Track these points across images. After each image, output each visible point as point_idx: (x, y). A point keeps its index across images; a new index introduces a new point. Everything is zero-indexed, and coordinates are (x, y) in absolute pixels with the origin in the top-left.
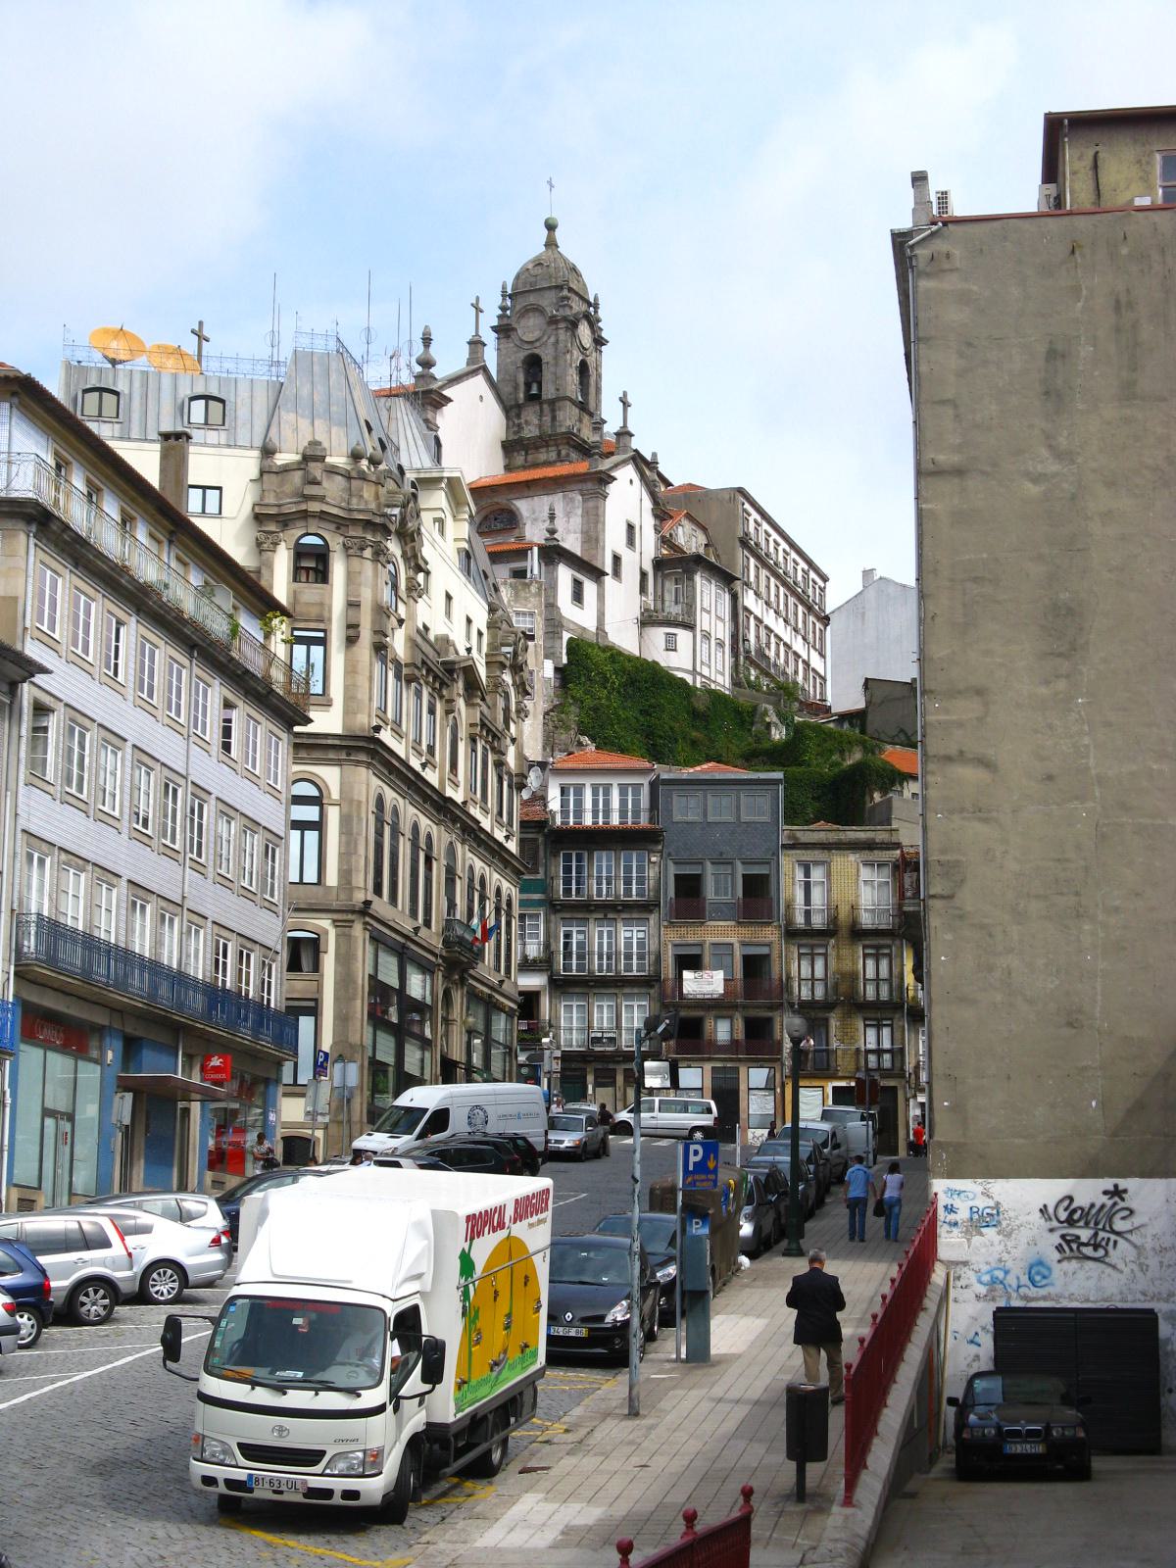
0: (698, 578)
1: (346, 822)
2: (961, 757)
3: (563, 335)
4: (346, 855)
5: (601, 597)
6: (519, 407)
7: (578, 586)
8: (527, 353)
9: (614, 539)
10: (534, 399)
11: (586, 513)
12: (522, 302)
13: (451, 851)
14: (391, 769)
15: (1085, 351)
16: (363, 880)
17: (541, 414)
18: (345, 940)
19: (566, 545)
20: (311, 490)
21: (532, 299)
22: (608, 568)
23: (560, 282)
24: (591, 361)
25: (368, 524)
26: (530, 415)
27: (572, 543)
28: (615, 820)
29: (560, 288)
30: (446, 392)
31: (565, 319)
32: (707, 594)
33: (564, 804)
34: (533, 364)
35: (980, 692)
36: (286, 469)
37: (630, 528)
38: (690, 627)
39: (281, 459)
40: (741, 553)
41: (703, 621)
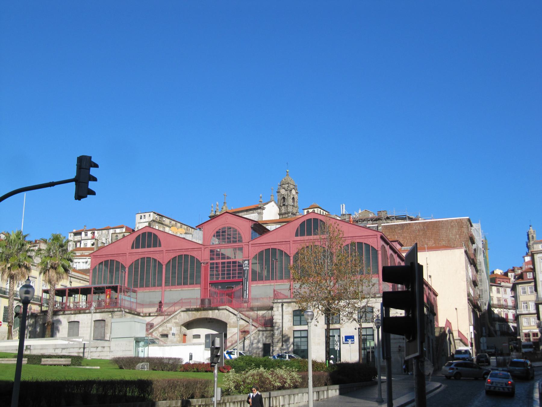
10: (284, 205)
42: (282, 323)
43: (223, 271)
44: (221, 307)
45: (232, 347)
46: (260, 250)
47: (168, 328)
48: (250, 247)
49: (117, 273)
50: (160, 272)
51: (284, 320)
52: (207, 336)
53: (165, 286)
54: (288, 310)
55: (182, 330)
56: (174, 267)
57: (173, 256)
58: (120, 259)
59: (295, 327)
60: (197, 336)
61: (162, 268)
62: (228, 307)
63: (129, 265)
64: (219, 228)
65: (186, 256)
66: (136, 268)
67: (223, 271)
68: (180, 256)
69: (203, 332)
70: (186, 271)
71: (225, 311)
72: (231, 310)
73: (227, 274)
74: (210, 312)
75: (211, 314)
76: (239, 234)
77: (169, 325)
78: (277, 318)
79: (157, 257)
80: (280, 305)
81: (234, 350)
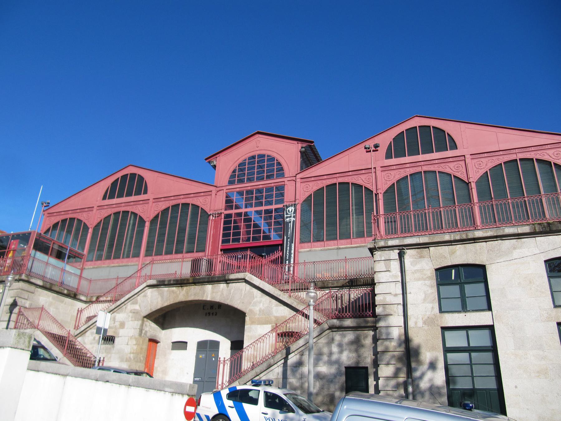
43: (248, 233)
44: (232, 276)
45: (251, 375)
46: (316, 188)
47: (117, 324)
48: (298, 184)
49: (69, 235)
50: (141, 233)
51: (410, 297)
52: (202, 346)
54: (418, 267)
55: (146, 329)
56: (163, 224)
57: (164, 207)
58: (83, 217)
59: (447, 316)
60: (181, 345)
61: (144, 226)
62: (249, 276)
63: (95, 224)
64: (243, 158)
65: (186, 205)
66: (105, 229)
67: (248, 233)
68: (176, 206)
69: (194, 335)
70: (182, 230)
71: (243, 286)
72: (256, 281)
73: (257, 198)
74: (209, 287)
75: (210, 293)
76: (279, 164)
78: (387, 292)
79: (139, 210)
80: (395, 254)
81: (257, 384)
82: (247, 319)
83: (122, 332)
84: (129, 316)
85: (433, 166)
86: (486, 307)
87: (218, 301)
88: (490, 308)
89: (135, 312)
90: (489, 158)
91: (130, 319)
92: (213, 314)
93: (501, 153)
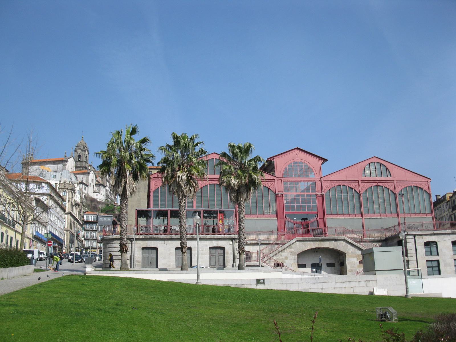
0: (101, 186)
1: (68, 221)
2: (130, 220)
3: (84, 152)
4: (68, 225)
5: (88, 189)
6: (77, 162)
7: (85, 187)
8: (78, 154)
9: (90, 181)
10: (79, 161)
11: (86, 178)
12: (78, 148)
13: (76, 224)
14: (72, 215)
15: (141, 188)
16: (69, 227)
17: (80, 163)
18: (67, 233)
19: (84, 182)
20: (65, 186)
21: (80, 147)
22: (89, 185)
23: (83, 145)
24: (87, 156)
25: (71, 190)
26: (79, 163)
27: (84, 182)
28: (92, 220)
29: (83, 146)
30: (68, 160)
31: (84, 150)
32: (102, 188)
33: (86, 218)
34: (79, 156)
35: (132, 215)
36: (62, 183)
37: (92, 180)
38: (100, 193)
39: (61, 182)
40: (106, 181)
41: (101, 192)
42: (116, 251)
53: (171, 217)
77: (284, 254)
82: (346, 255)
83: (286, 261)
84: (289, 254)
85: (345, 183)
86: (437, 254)
87: (333, 248)
88: (438, 255)
89: (291, 252)
90: (331, 183)
91: (290, 255)
92: (316, 252)
93: (407, 182)
